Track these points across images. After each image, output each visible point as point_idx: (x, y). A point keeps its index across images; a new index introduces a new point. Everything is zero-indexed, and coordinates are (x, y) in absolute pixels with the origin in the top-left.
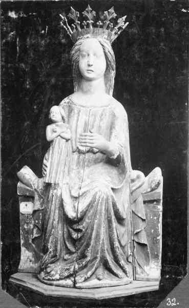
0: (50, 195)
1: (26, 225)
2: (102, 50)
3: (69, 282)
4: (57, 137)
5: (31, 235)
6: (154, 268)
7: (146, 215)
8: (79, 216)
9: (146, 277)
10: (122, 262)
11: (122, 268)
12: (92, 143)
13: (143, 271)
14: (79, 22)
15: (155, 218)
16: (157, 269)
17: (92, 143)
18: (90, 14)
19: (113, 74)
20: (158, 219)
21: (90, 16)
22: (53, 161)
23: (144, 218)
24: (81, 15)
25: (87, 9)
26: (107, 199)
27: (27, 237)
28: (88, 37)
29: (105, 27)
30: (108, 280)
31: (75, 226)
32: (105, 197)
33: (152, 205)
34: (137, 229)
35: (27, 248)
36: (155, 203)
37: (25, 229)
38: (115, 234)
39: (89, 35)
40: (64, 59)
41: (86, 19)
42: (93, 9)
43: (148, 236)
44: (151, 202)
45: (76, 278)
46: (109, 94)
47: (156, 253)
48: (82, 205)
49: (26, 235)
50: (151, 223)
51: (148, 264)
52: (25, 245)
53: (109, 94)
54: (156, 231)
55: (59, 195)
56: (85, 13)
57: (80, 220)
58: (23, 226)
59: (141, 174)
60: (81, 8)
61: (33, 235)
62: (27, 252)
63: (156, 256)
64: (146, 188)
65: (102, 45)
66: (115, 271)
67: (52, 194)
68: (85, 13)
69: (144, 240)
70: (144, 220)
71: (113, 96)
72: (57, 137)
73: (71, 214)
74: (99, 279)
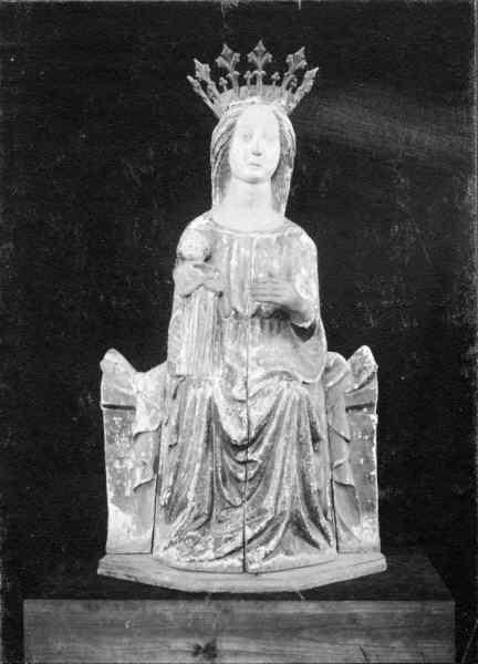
0: (190, 398)
1: (117, 462)
2: (277, 128)
3: (236, 561)
4: (197, 289)
5: (130, 482)
6: (366, 528)
7: (351, 434)
8: (253, 434)
9: (357, 545)
10: (323, 521)
11: (323, 531)
12: (276, 296)
13: (351, 535)
14: (237, 73)
15: (367, 437)
16: (374, 530)
17: (276, 296)
18: (260, 57)
19: (288, 173)
20: (371, 439)
21: (260, 62)
22: (186, 328)
23: (348, 437)
24: (244, 60)
25: (257, 49)
26: (300, 402)
27: (121, 485)
28: (253, 103)
29: (260, 82)
30: (303, 555)
31: (241, 456)
32: (298, 399)
33: (359, 414)
34: (338, 459)
35: (123, 509)
36: (365, 410)
37: (115, 470)
38: (278, 466)
39: (255, 99)
40: (459, 182)
41: (253, 67)
42: (269, 47)
43: (355, 471)
44: (359, 408)
45: (249, 555)
46: (278, 209)
47: (369, 501)
48: (257, 414)
49: (118, 482)
50: (354, 451)
51: (358, 523)
52: (117, 502)
53: (278, 209)
54: (368, 461)
55: (207, 397)
56: (251, 56)
57: (251, 442)
58: (111, 464)
59: (341, 358)
60: (243, 47)
61: (134, 480)
62: (120, 513)
63: (369, 508)
64: (351, 384)
65: (277, 116)
66: (314, 537)
67: (195, 399)
68: (251, 56)
69: (349, 480)
70: (347, 441)
71: (210, 208)
72: (197, 289)
73: (237, 434)
74: (287, 553)
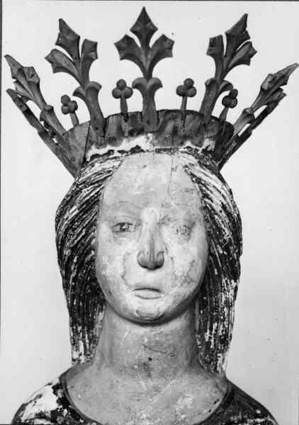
28: (136, 150)
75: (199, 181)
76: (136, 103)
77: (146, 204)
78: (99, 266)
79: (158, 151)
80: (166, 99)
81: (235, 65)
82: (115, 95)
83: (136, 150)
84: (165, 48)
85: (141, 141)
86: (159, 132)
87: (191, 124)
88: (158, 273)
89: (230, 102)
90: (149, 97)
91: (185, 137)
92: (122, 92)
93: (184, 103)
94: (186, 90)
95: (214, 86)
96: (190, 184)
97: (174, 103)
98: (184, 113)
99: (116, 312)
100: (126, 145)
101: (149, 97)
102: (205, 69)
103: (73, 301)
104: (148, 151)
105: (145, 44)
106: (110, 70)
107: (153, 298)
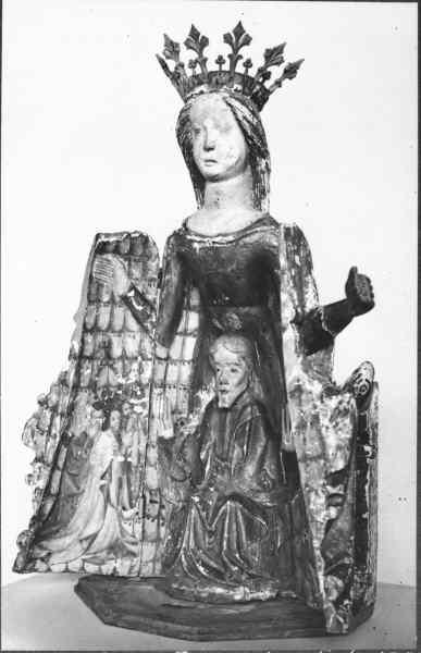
28: (202, 92)
75: (229, 105)
76: (198, 70)
77: (206, 117)
78: (74, 525)
79: (211, 92)
80: (212, 66)
81: (241, 46)
82: (217, 62)
83: (202, 92)
84: (248, 41)
85: (203, 88)
86: (209, 83)
87: (225, 78)
88: (211, 152)
89: (248, 64)
90: (233, 65)
91: (223, 84)
92: (192, 65)
93: (247, 71)
94: (220, 61)
95: (234, 58)
96: (225, 106)
97: (216, 68)
98: (221, 71)
99: (165, 377)
100: (197, 90)
101: (233, 65)
102: (258, 62)
103: (52, 509)
104: (143, 526)
105: (238, 38)
106: (217, 49)
107: (218, 236)
